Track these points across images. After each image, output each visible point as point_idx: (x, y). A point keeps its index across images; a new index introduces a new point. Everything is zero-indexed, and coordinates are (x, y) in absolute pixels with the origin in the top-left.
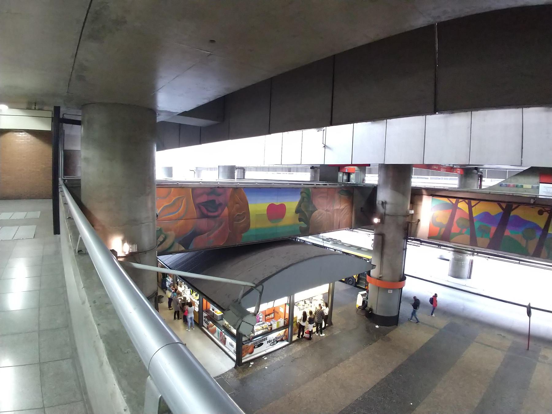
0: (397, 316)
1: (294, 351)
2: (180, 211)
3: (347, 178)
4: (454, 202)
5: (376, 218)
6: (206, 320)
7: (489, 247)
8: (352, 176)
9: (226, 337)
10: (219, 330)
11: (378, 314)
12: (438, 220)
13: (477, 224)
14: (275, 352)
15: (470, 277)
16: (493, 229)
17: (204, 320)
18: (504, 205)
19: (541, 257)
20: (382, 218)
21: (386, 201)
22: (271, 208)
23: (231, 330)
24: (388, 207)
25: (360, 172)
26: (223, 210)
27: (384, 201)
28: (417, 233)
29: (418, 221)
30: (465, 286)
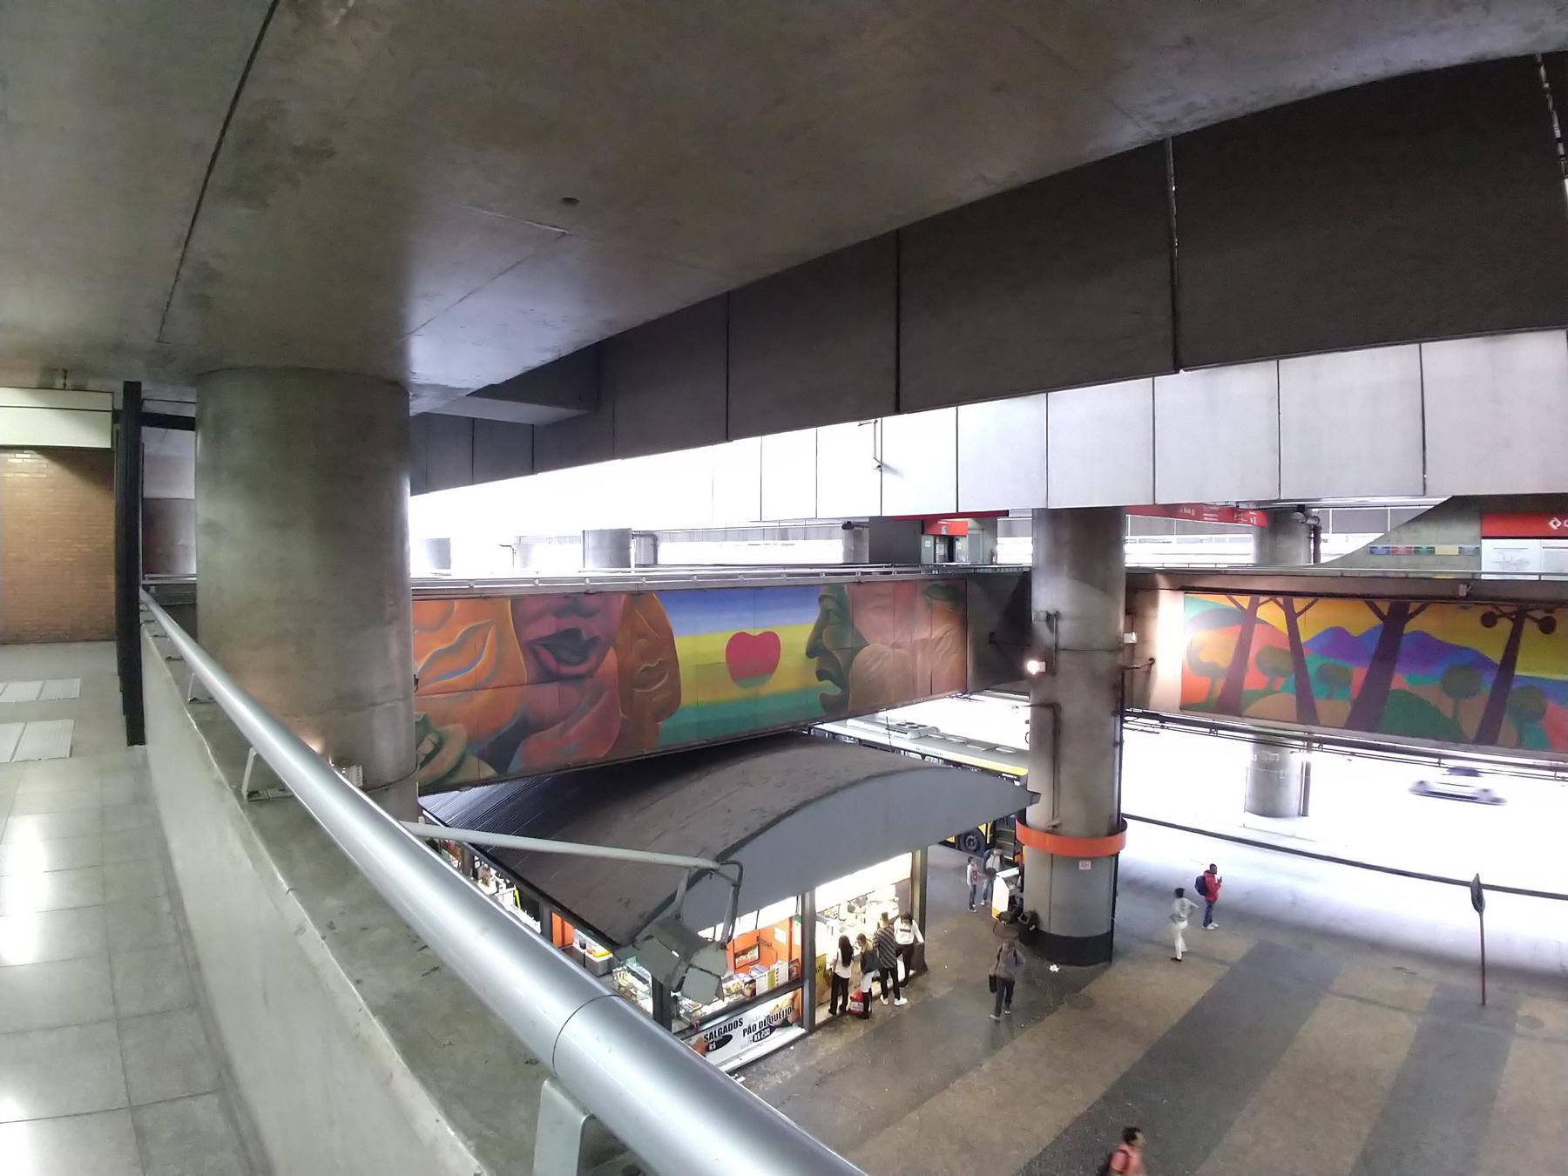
7: (1351, 725)
8: (961, 546)
13: (1313, 663)
14: (767, 1061)
15: (1305, 814)
16: (1359, 673)
18: (1384, 607)
24: (1064, 626)
27: (1051, 612)
29: (1151, 662)
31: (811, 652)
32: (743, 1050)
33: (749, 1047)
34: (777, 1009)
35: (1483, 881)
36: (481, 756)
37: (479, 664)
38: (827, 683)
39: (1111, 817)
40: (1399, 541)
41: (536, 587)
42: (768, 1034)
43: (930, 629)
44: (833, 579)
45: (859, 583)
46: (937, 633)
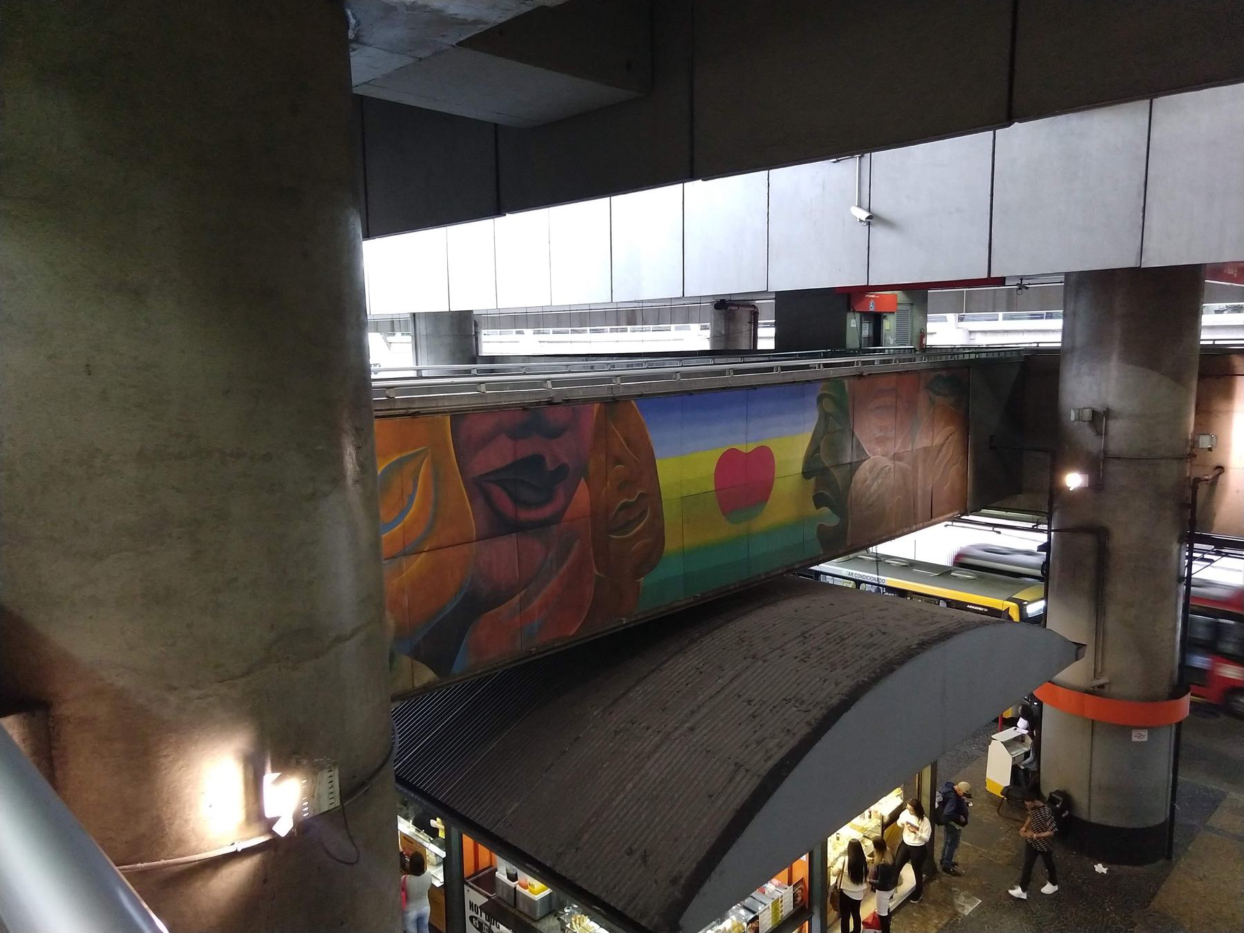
0: (1163, 824)
5: (1067, 473)
6: (483, 917)
8: (888, 325)
11: (1095, 818)
17: (471, 918)
20: (1096, 466)
21: (1108, 409)
24: (1116, 427)
25: (912, 309)
26: (570, 496)
27: (1098, 408)
28: (1214, 515)
31: (806, 474)
36: (416, 655)
37: (407, 518)
39: (1172, 673)
41: (483, 395)
43: (931, 434)
44: (832, 372)
45: (860, 376)
46: (938, 440)
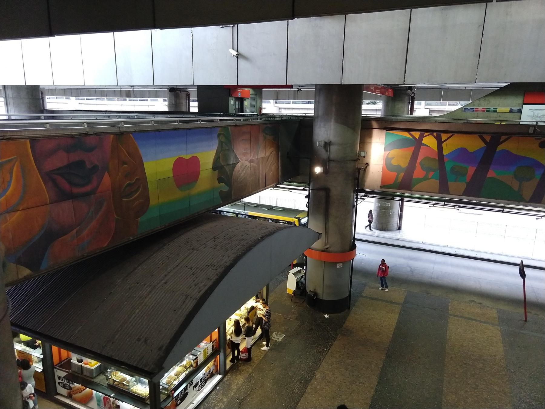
1: (234, 387)
2: (8, 193)
3: (240, 106)
4: (417, 137)
7: (465, 194)
8: (247, 103)
9: (120, 403)
10: (101, 394)
12: (394, 162)
13: (449, 166)
14: (207, 400)
15: (400, 229)
16: (471, 170)
18: (488, 138)
19: (542, 203)
20: (325, 164)
22: (179, 163)
23: (129, 389)
24: (333, 148)
27: (327, 141)
29: (366, 165)
30: (502, 255)
31: (214, 169)
32: (194, 398)
33: (196, 395)
34: (208, 369)
35: (524, 263)
38: (223, 184)
40: (479, 105)
41: (48, 130)
42: (204, 384)
43: (264, 152)
44: (224, 124)
45: (235, 126)
